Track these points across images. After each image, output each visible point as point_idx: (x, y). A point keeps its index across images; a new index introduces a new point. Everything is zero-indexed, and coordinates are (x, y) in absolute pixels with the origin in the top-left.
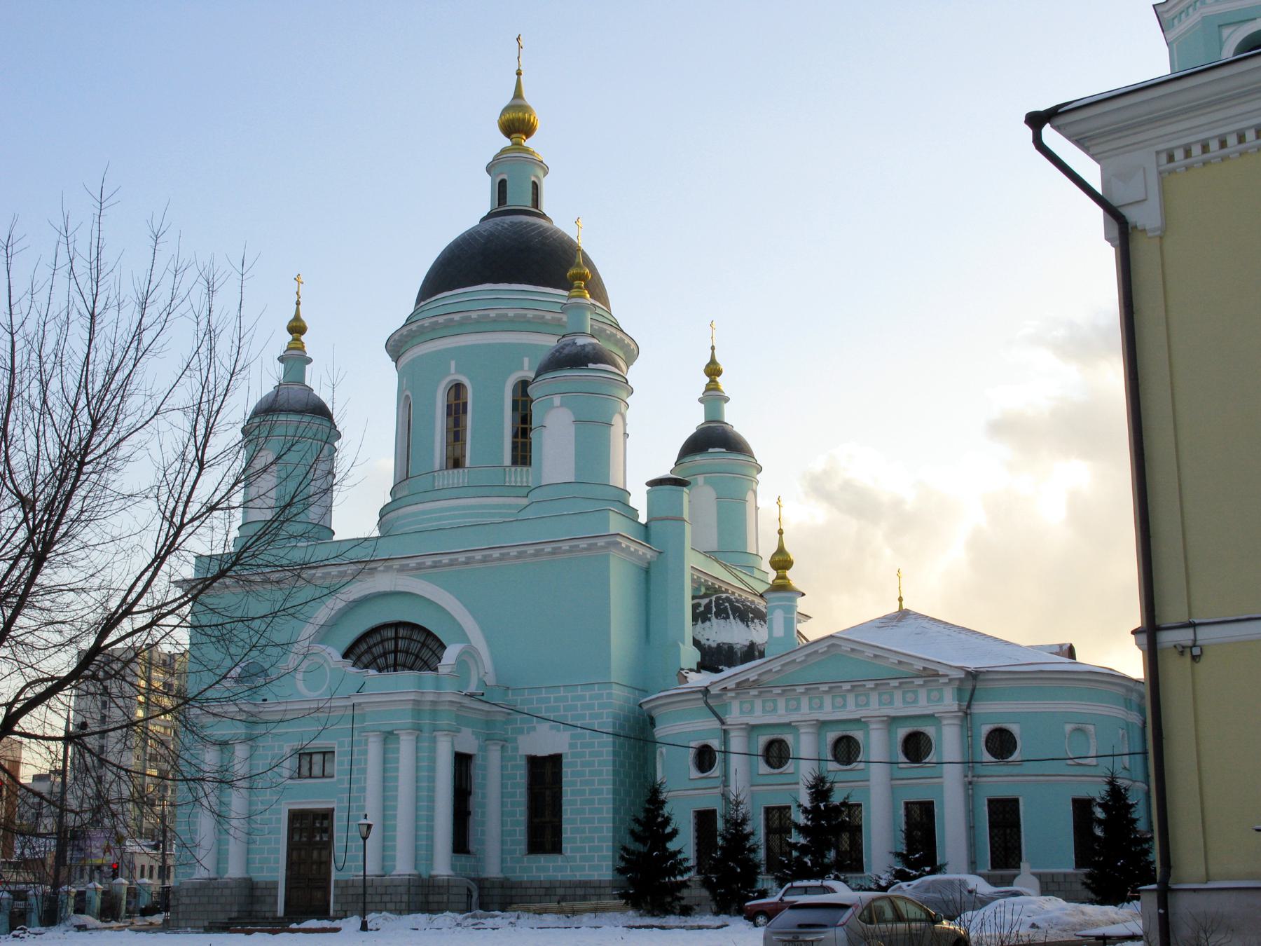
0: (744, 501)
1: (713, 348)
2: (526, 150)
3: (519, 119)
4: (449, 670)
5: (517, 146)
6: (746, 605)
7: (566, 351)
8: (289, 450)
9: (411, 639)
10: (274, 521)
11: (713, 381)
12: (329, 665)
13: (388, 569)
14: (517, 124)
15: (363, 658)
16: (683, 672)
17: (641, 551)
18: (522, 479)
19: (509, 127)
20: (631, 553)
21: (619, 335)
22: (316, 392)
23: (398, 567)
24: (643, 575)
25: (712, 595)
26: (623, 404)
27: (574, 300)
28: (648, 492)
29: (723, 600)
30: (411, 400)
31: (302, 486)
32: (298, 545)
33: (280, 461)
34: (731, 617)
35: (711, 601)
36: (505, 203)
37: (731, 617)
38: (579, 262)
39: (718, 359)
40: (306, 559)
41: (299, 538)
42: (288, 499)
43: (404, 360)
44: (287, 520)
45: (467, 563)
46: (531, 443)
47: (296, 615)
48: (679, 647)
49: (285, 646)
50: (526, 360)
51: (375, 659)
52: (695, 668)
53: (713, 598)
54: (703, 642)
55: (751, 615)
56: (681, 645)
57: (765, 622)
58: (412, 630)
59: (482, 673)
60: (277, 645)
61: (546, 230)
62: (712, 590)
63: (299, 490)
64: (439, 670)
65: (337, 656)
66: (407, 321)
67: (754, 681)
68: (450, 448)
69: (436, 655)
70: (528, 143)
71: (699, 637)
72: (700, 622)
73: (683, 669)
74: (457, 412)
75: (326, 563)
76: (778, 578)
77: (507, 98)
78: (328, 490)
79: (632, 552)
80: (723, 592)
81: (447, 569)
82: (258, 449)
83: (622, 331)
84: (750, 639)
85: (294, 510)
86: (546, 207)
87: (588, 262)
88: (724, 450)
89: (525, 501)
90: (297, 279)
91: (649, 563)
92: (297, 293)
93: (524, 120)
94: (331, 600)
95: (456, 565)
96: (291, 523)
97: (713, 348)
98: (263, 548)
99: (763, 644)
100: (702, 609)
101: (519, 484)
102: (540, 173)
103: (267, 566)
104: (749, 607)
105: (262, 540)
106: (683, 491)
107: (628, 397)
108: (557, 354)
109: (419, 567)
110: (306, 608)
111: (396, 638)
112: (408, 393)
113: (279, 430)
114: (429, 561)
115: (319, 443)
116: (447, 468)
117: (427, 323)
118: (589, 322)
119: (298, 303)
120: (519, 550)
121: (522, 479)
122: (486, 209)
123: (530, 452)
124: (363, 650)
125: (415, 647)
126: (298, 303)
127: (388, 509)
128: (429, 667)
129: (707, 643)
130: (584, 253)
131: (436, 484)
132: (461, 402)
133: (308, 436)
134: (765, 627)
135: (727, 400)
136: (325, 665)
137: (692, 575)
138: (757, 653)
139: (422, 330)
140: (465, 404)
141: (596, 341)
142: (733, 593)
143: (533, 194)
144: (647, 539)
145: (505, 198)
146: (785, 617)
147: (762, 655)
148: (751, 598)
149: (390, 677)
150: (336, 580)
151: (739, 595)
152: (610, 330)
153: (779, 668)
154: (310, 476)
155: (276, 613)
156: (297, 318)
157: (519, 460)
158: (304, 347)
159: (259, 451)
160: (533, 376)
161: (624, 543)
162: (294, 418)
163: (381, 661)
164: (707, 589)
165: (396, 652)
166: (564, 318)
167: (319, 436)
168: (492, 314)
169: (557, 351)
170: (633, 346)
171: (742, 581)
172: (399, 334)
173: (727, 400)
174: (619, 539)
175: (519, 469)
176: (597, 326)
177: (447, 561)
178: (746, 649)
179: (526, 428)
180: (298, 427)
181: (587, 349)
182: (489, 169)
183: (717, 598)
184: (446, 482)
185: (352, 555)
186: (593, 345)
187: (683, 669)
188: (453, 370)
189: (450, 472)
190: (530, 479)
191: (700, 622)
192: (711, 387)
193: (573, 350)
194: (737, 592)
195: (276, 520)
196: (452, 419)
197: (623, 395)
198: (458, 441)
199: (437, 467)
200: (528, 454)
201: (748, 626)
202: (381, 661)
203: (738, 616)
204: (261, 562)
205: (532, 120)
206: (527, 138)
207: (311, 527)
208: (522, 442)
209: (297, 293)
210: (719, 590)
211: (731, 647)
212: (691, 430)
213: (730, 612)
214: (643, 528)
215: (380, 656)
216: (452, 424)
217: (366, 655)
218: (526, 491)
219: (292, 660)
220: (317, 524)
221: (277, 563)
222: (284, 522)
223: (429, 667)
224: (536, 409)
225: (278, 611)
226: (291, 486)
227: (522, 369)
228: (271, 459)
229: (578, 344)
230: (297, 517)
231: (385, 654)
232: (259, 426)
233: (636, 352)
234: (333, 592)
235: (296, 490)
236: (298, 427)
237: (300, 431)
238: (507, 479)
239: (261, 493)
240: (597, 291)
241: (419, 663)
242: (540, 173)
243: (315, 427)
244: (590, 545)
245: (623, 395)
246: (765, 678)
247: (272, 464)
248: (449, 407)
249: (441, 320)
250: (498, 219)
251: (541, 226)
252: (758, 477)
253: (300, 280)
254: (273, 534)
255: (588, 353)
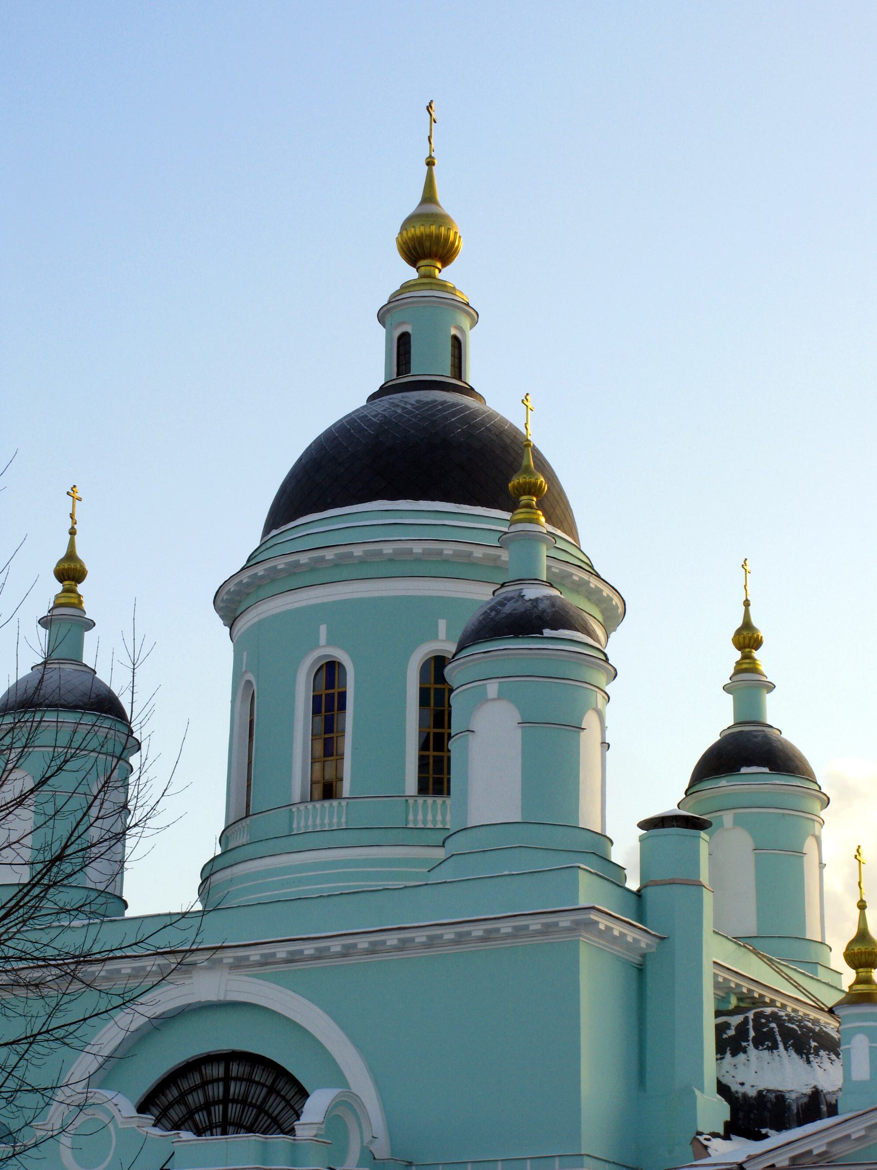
0: (800, 854)
1: (747, 603)
2: (442, 286)
3: (430, 236)
4: (314, 1132)
5: (428, 280)
6: (806, 1027)
7: (507, 609)
8: (60, 769)
9: (250, 1081)
10: (34, 886)
11: (747, 657)
12: (116, 1127)
13: (214, 964)
14: (427, 244)
15: (172, 1111)
16: (701, 1138)
17: (631, 935)
18: (434, 817)
19: (415, 248)
20: (615, 940)
21: (594, 582)
22: (102, 675)
23: (231, 960)
24: (634, 972)
25: (748, 1010)
26: (600, 696)
27: (520, 527)
28: (642, 839)
29: (766, 1017)
30: (255, 687)
31: (81, 828)
32: (74, 924)
33: (45, 787)
34: (781, 1046)
35: (746, 1019)
36: (408, 371)
37: (781, 1046)
38: (529, 466)
39: (755, 622)
40: (86, 948)
41: (73, 913)
42: (56, 848)
43: (244, 623)
44: (55, 884)
45: (344, 955)
46: (449, 758)
47: (66, 1040)
48: (694, 1092)
49: (46, 1092)
50: (442, 624)
51: (191, 1113)
52: (721, 1131)
53: (751, 1015)
54: (734, 1087)
55: (813, 1044)
56: (697, 1093)
57: (837, 1055)
58: (253, 1067)
59: (367, 1138)
60: (34, 1090)
61: (475, 414)
62: (748, 1001)
63: (76, 834)
64: (298, 1132)
65: (128, 1108)
66: (248, 561)
67: (819, 1155)
68: (318, 766)
69: (292, 1108)
70: (446, 274)
71: (725, 1081)
72: (728, 1055)
73: (701, 1134)
74: (329, 708)
75: (118, 953)
76: (858, 982)
77: (411, 203)
78: (120, 837)
79: (615, 937)
80: (766, 1005)
81: (539, 940)
82: (10, 766)
83: (598, 576)
84: (814, 1083)
85: (67, 868)
86: (473, 376)
87: (542, 465)
88: (766, 770)
89: (440, 854)
90: (72, 493)
91: (644, 956)
92: (72, 516)
93: (438, 237)
94: (122, 1014)
95: (495, 939)
96: (61, 889)
97: (747, 603)
98: (14, 930)
99: (834, 1093)
100: (731, 1032)
101: (430, 826)
102: (465, 323)
103: (21, 959)
104: (811, 1030)
105: (13, 917)
106: (699, 837)
107: (608, 683)
108: (493, 614)
109: (266, 962)
110: (85, 1028)
111: (227, 1080)
112: (250, 677)
113: (45, 737)
114: (281, 952)
115: (110, 758)
116: (311, 800)
117: (281, 563)
118: (544, 562)
119: (73, 532)
120: (429, 933)
121: (434, 817)
122: (376, 379)
123: (449, 773)
124: (171, 1098)
125: (257, 1094)
126: (73, 532)
127: (218, 865)
128: (279, 1126)
129: (742, 1090)
130: (536, 451)
131: (295, 825)
132: (336, 691)
133: (90, 747)
134: (838, 1063)
135: (770, 687)
136: (111, 1126)
137: (716, 975)
138: (824, 1108)
139: (273, 576)
140: (343, 696)
141: (557, 593)
142: (784, 1007)
143: (453, 356)
144: (641, 916)
145: (408, 363)
146: (870, 1047)
147: (833, 1110)
148: (814, 1015)
149: (215, 1143)
150: (133, 983)
151: (794, 1010)
152: (578, 575)
153: (863, 1133)
154: (94, 812)
155: (36, 1035)
156: (71, 555)
157: (431, 786)
158: (81, 602)
159: (11, 771)
160: (454, 651)
161: (603, 923)
162: (70, 718)
163: (200, 1118)
164: (740, 999)
165: (226, 1100)
166: (504, 555)
167: (109, 747)
168: (388, 549)
169: (492, 609)
170: (616, 601)
171: (797, 986)
172: (236, 580)
173: (770, 687)
174: (594, 916)
175: (430, 800)
176: (557, 567)
177: (312, 952)
178: (805, 1100)
179: (443, 734)
180: (75, 732)
181: (541, 606)
182: (383, 316)
183: (755, 1014)
184: (318, 821)
185: (161, 941)
186: (550, 598)
187: (701, 1134)
188: (323, 640)
189: (318, 805)
190: (448, 817)
191: (728, 1055)
192: (744, 666)
193: (520, 607)
194: (791, 1006)
195: (38, 883)
196: (320, 719)
197: (600, 679)
198: (332, 755)
199: (297, 797)
200: (445, 777)
201: (809, 1062)
202: (200, 1118)
203: (792, 1045)
204: (11, 953)
205: (452, 238)
206: (444, 265)
207: (94, 895)
208: (434, 757)
209: (72, 516)
210: (759, 1002)
211: (780, 1097)
212: (713, 738)
213: (779, 1038)
214: (634, 897)
215: (198, 1110)
216: (321, 727)
217: (176, 1107)
218: (440, 837)
219: (55, 1116)
220: (102, 892)
221: (36, 954)
222: (49, 887)
223: (279, 1126)
224: (457, 701)
225: (39, 1033)
226: (63, 828)
227: (436, 638)
228: (30, 784)
229: (527, 598)
230: (71, 879)
231: (207, 1106)
232: (12, 729)
233: (621, 610)
234: (127, 1001)
235: (71, 835)
236: (75, 732)
237: (78, 738)
238: (411, 817)
239: (12, 840)
240: (558, 511)
241: (264, 1121)
242: (465, 323)
243: (102, 732)
244: (547, 926)
245: (600, 679)
246: (836, 1149)
247: (32, 791)
248: (316, 699)
249: (304, 558)
250: (398, 396)
251: (467, 408)
252: (824, 814)
253: (77, 495)
254: (32, 907)
255: (544, 611)
